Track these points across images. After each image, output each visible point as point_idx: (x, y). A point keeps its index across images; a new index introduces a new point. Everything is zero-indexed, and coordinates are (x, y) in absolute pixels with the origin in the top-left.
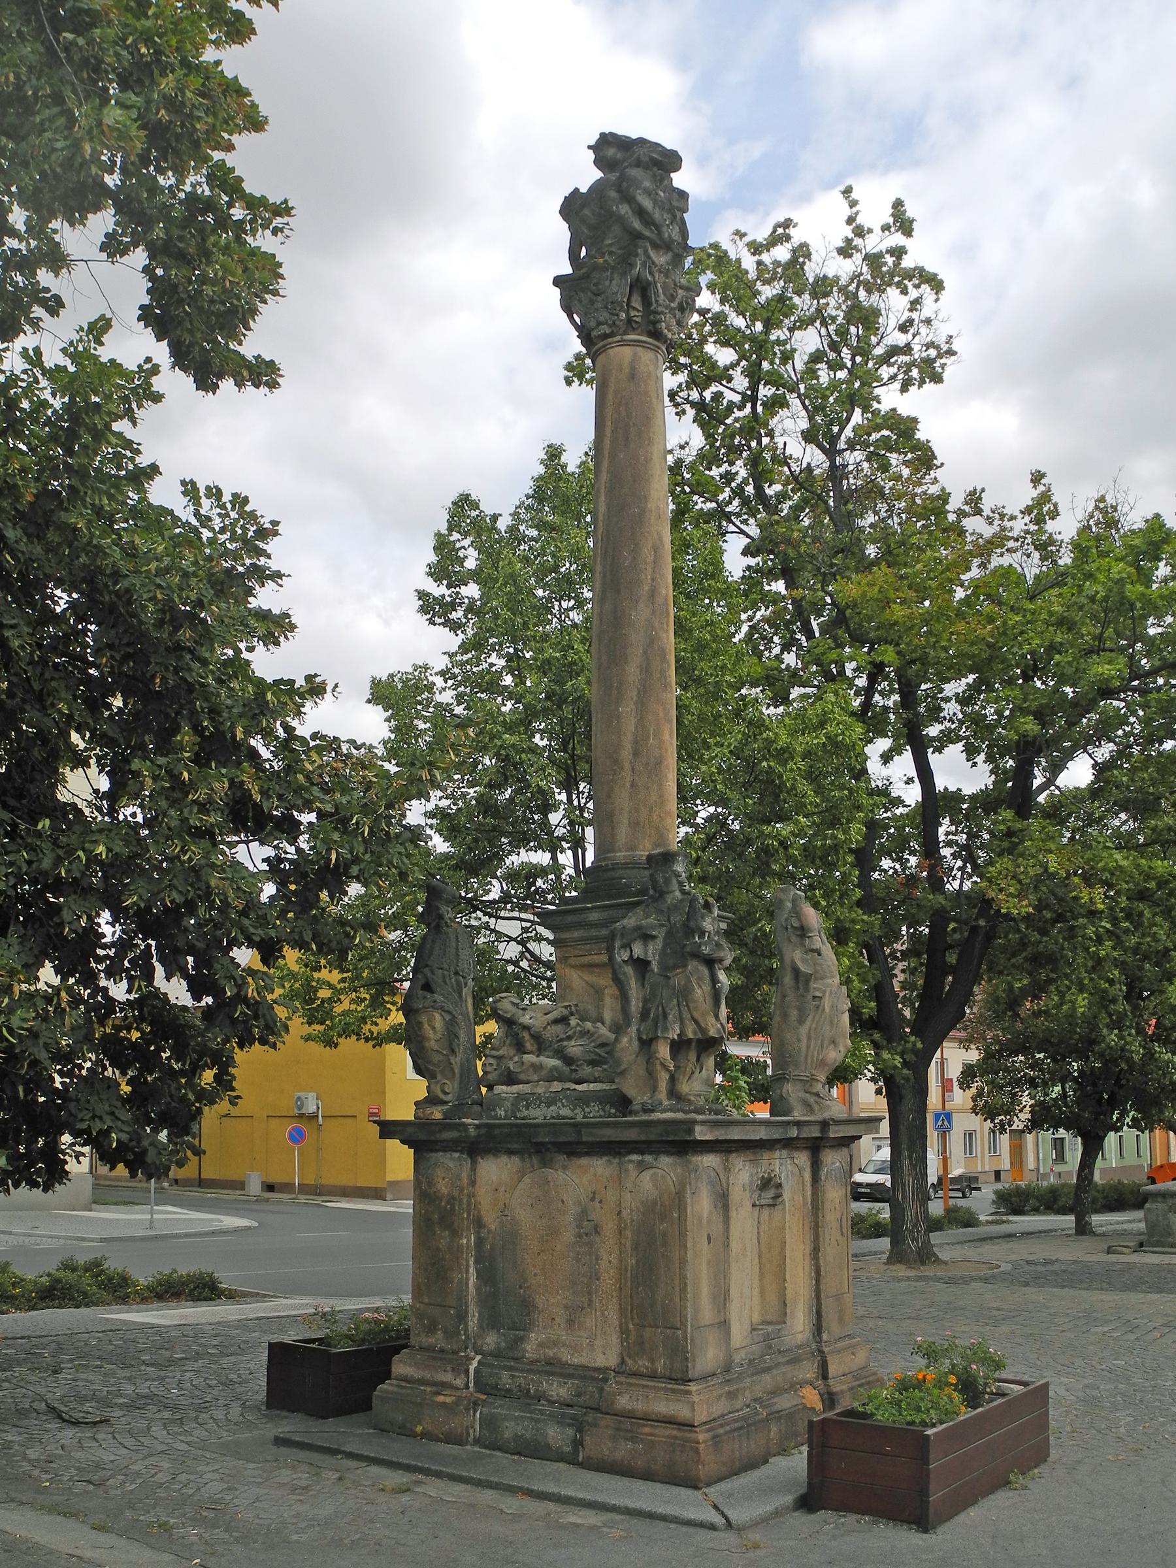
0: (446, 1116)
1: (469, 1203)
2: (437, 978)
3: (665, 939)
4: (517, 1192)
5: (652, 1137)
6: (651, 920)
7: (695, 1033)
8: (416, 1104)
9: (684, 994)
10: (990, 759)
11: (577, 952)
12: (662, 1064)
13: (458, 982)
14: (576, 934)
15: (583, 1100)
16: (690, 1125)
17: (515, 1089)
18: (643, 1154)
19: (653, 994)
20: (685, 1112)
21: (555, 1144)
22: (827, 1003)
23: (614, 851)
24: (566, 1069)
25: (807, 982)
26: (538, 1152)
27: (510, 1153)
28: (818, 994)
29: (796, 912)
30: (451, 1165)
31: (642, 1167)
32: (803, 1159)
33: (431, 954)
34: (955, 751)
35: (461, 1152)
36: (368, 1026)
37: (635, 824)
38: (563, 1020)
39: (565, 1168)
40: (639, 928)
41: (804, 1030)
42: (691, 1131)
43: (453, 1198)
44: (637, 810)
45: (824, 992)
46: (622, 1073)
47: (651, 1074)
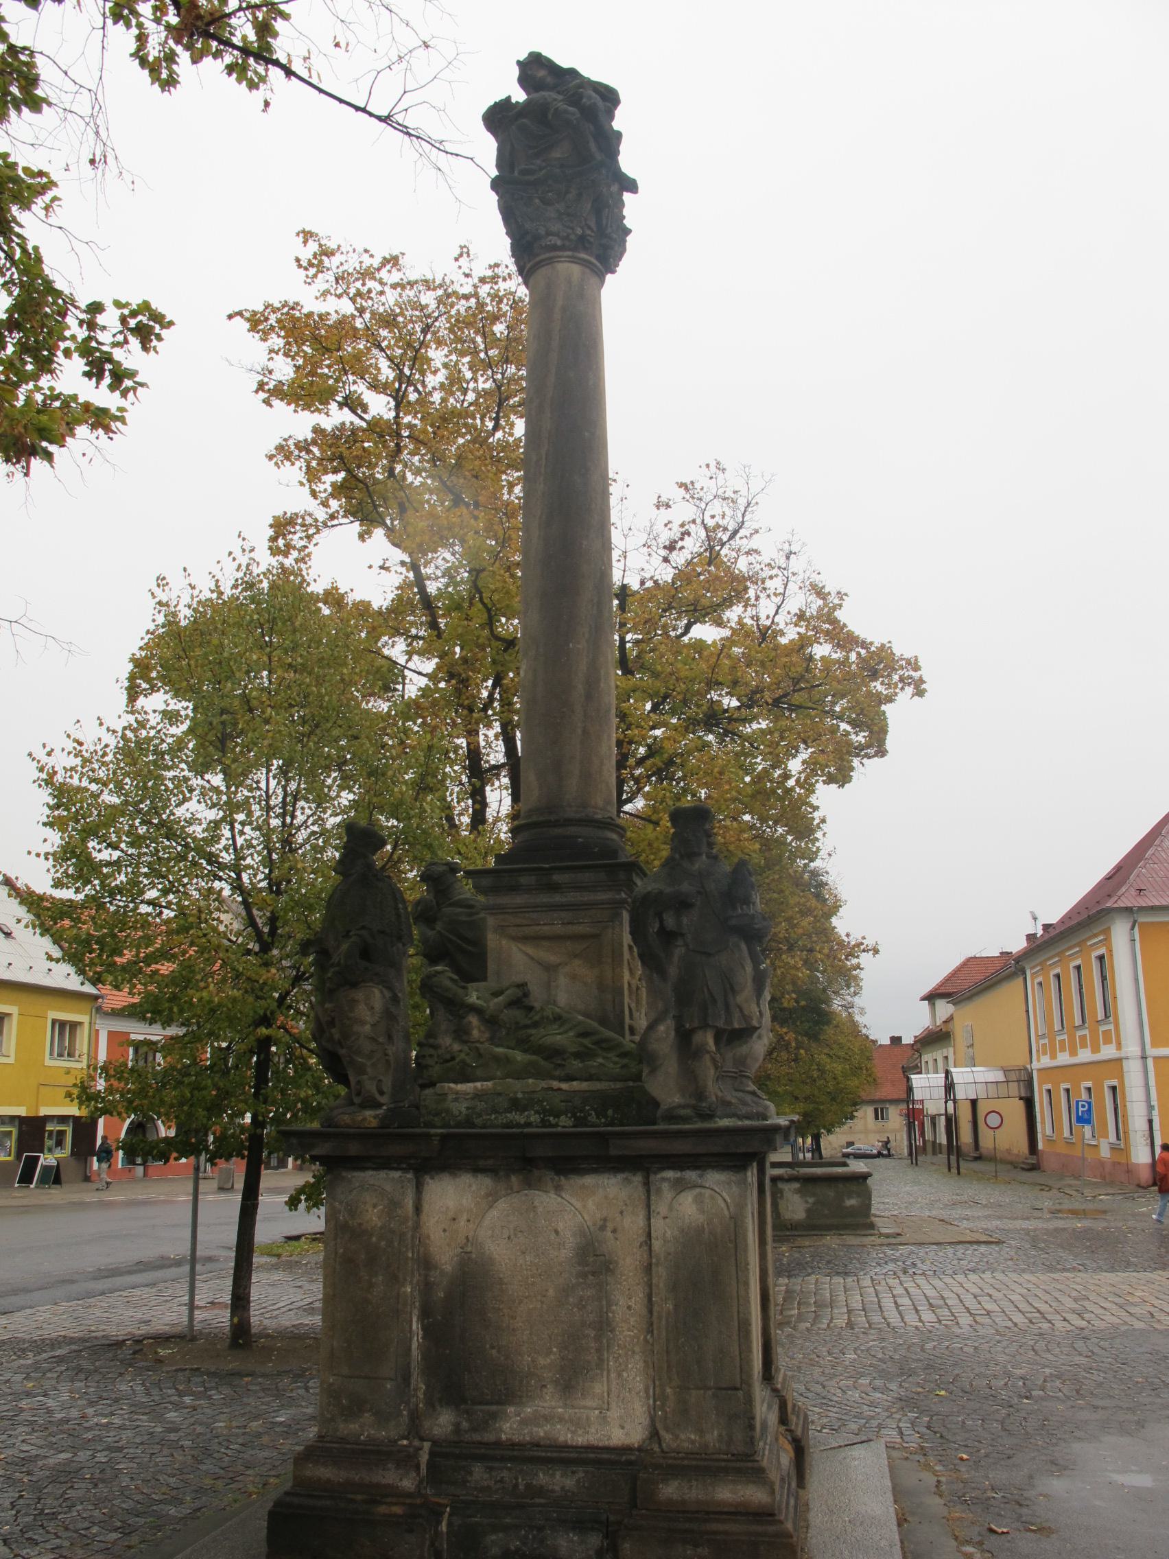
18: (682, 1169)
27: (477, 1170)
31: (680, 1186)
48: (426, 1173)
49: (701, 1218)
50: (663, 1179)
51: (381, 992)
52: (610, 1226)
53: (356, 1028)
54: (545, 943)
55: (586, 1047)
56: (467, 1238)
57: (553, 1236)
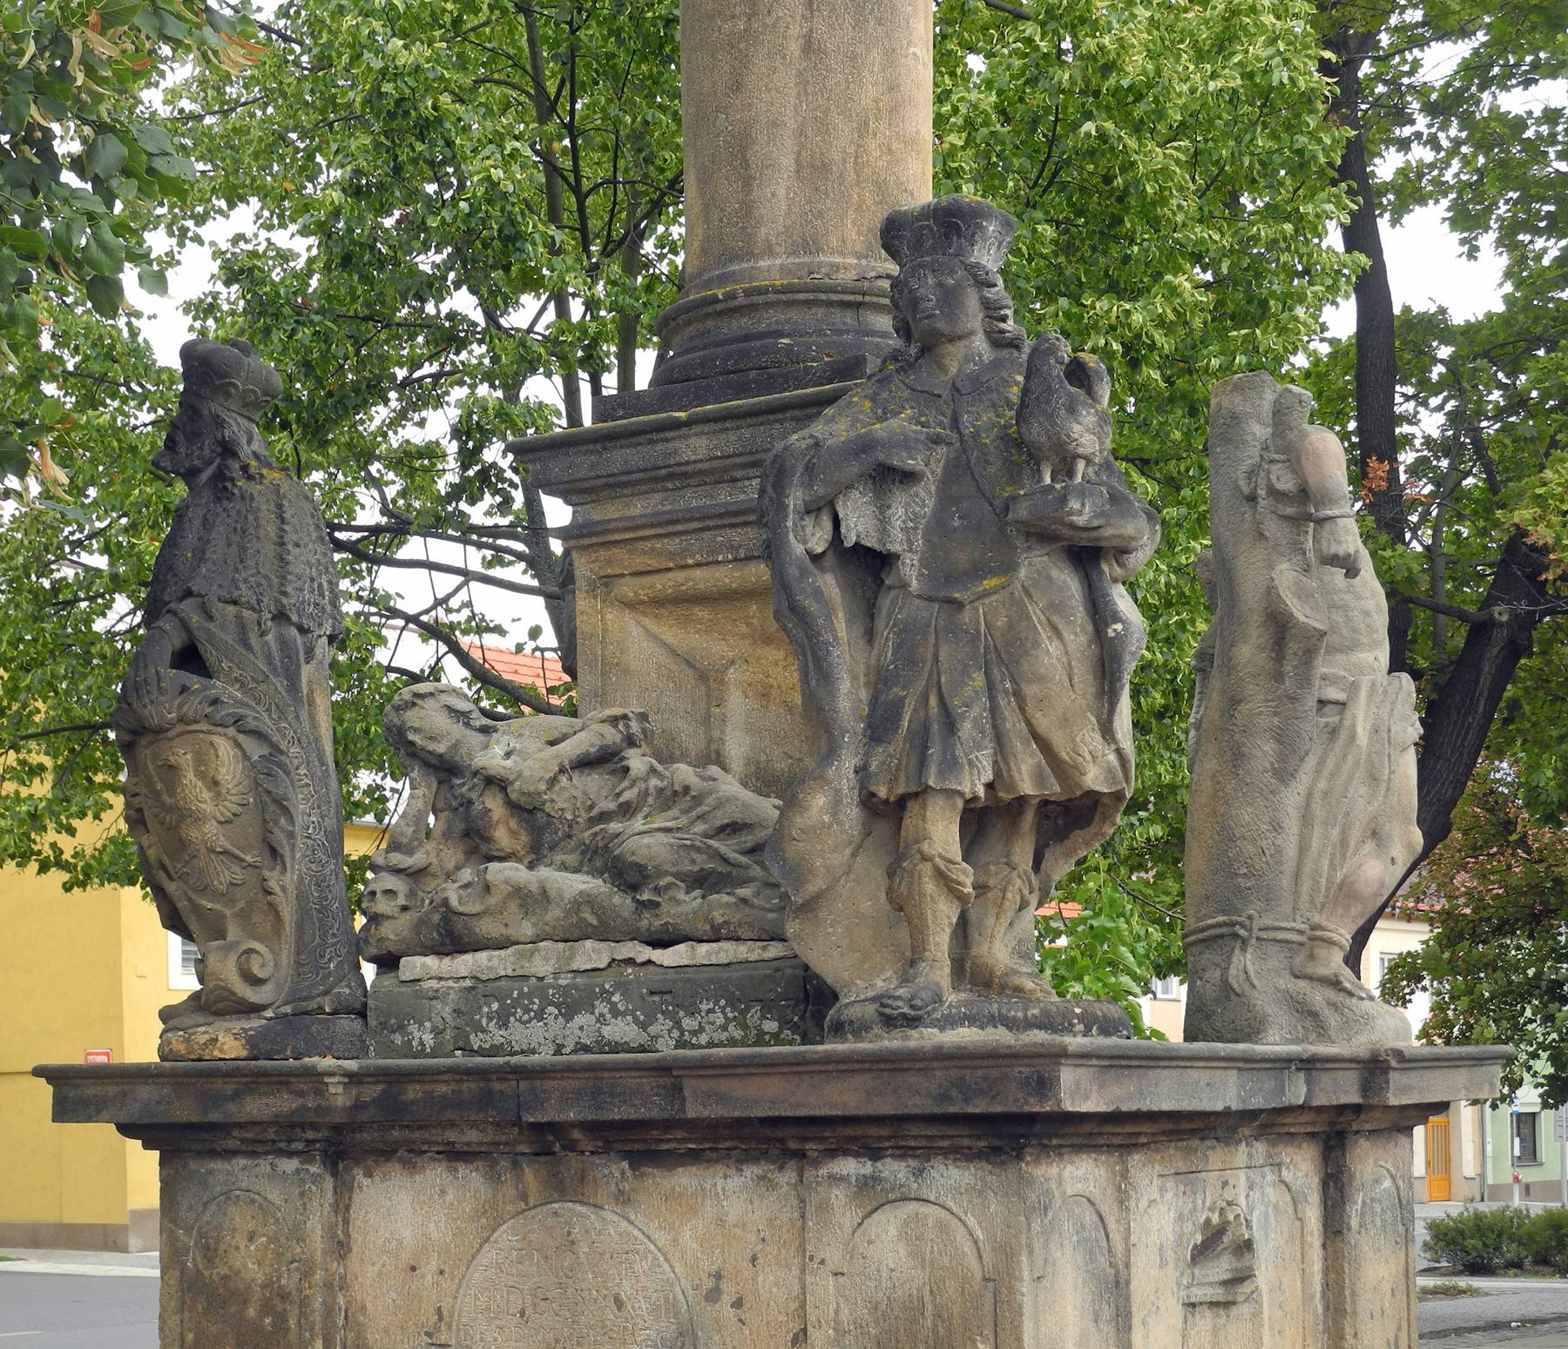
0: (257, 1047)
1: (329, 1311)
2: (218, 636)
3: (945, 483)
4: (476, 1275)
5: (917, 1104)
6: (901, 423)
7: (1040, 779)
8: (167, 1014)
9: (1005, 658)
10: (1507, 240)
11: (641, 562)
12: (941, 877)
13: (285, 645)
14: (638, 508)
15: (676, 994)
16: (1041, 1068)
17: (465, 963)
18: (875, 1155)
19: (908, 656)
20: (1011, 1024)
21: (593, 1128)
22: (1361, 720)
23: (750, 255)
24: (622, 903)
25: (1309, 654)
26: (544, 1152)
27: (455, 1155)
28: (1333, 693)
29: (1286, 448)
30: (275, 1195)
31: (872, 1196)
32: (1302, 1166)
33: (200, 557)
34: (1430, 218)
35: (305, 1155)
36: (51, 835)
37: (814, 170)
38: (603, 760)
39: (623, 1198)
40: (865, 446)
41: (1291, 799)
42: (1044, 1085)
43: (284, 1296)
44: (823, 124)
45: (1353, 688)
46: (809, 907)
47: (902, 907)
48: (357, 1162)
49: (918, 1278)
50: (835, 1179)
51: (238, 745)
52: (729, 1291)
53: (193, 834)
54: (701, 613)
55: (726, 861)
56: (439, 1311)
57: (611, 1313)
